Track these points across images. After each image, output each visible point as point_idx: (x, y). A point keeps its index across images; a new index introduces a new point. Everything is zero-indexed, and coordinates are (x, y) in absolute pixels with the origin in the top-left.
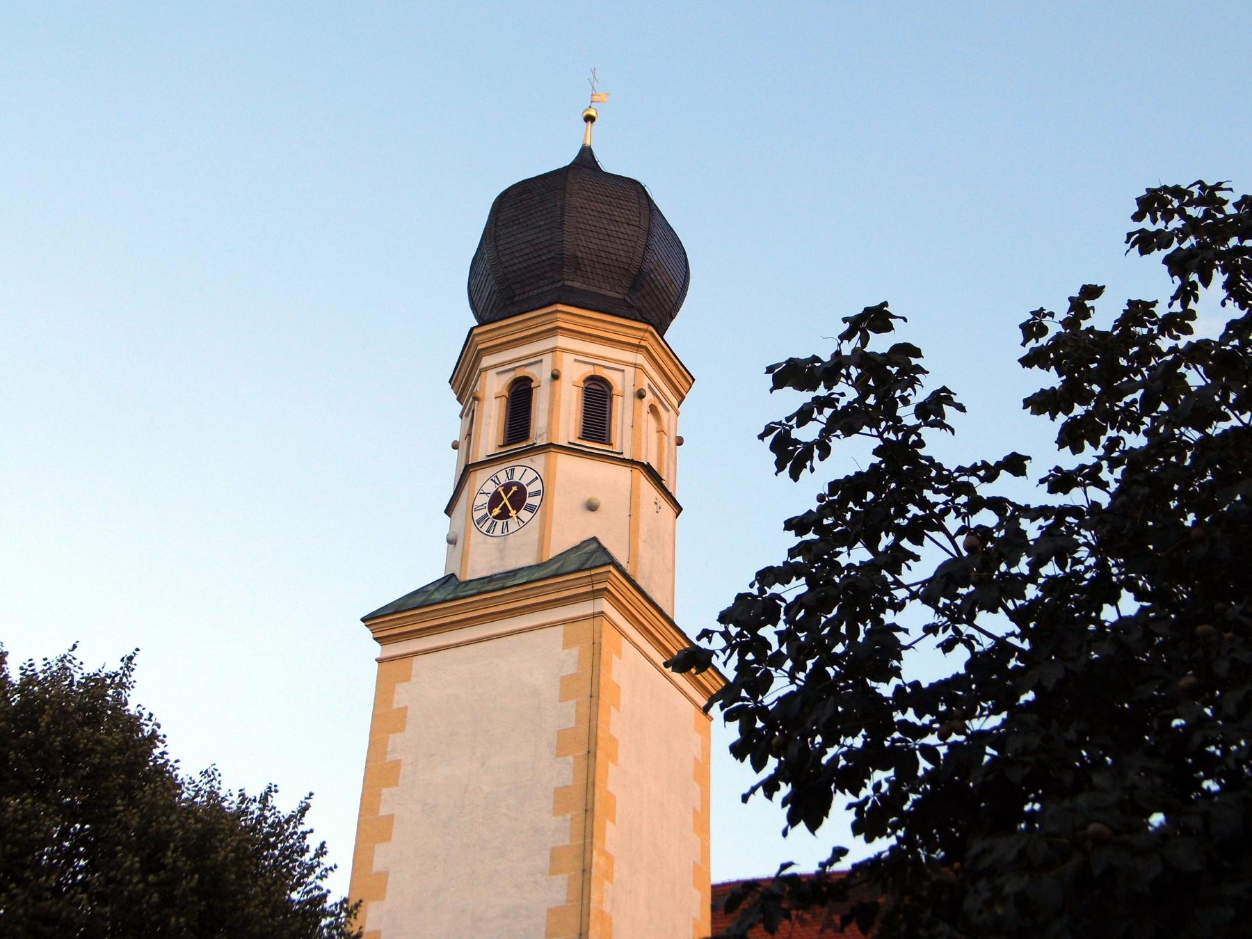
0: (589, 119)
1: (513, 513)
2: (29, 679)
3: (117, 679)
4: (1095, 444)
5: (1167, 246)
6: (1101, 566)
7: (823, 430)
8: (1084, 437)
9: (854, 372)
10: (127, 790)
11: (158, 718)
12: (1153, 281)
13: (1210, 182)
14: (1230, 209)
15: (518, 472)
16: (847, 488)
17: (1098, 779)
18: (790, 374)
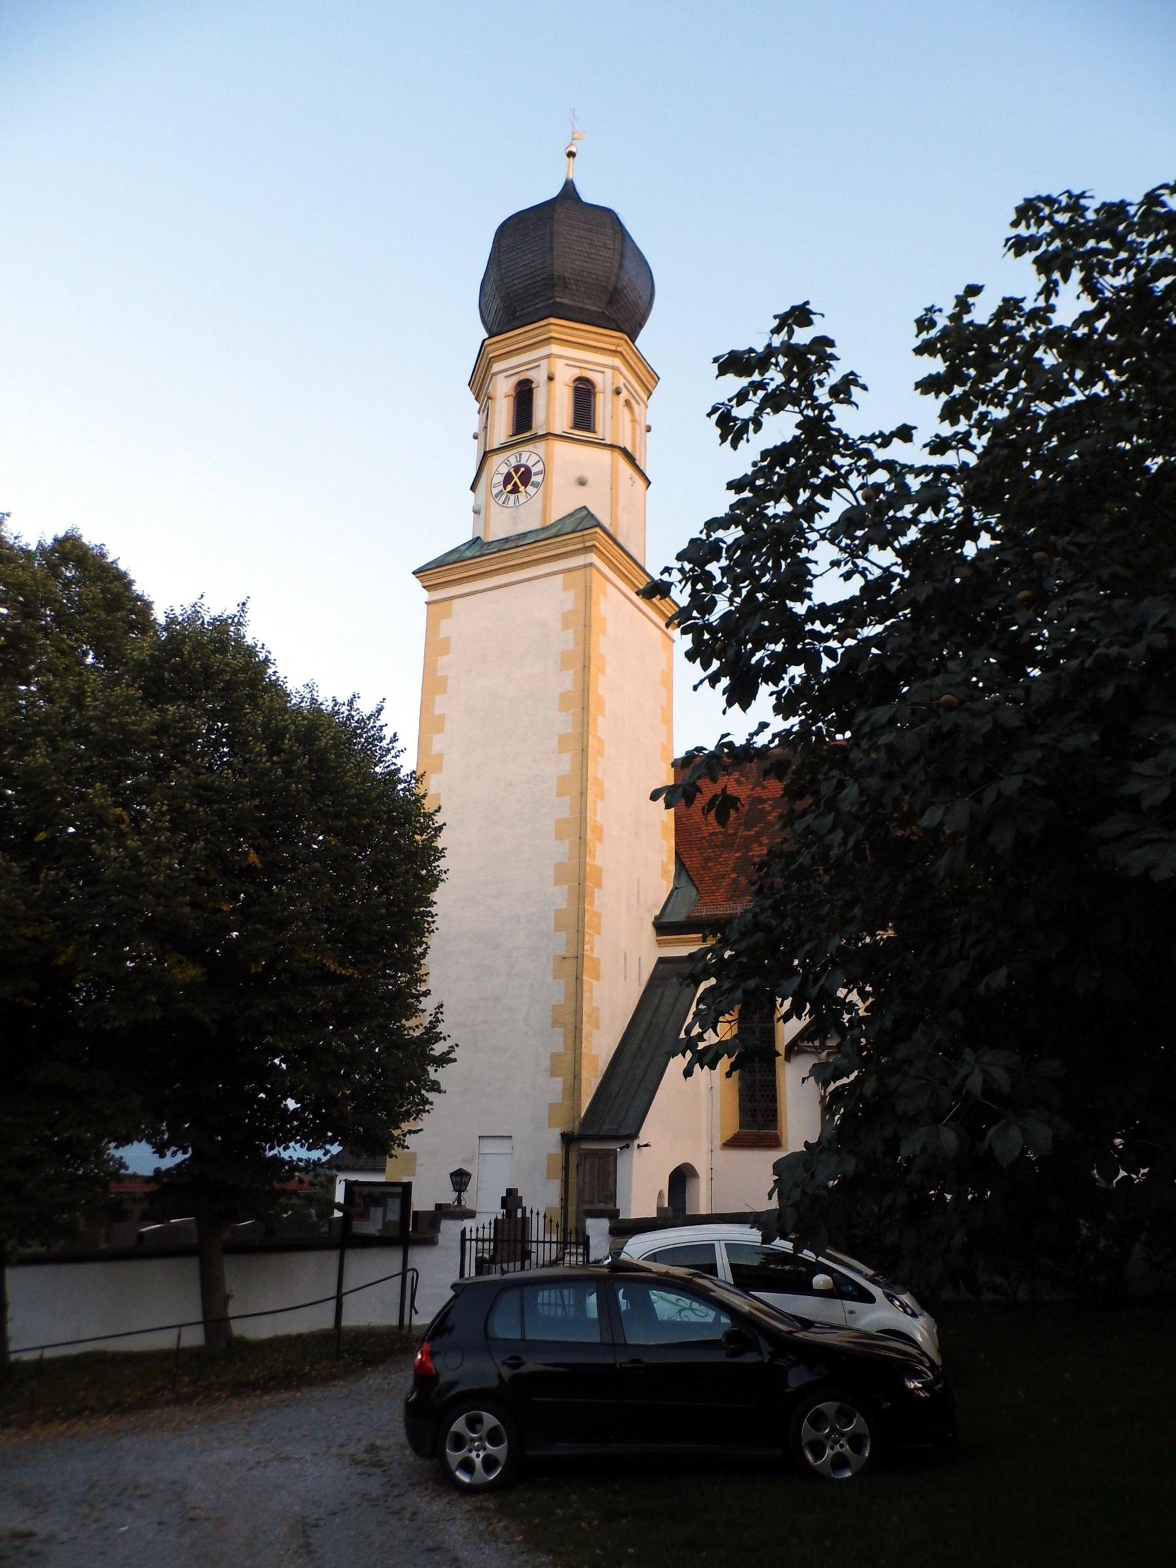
0: (571, 155)
1: (522, 488)
2: (172, 621)
3: (236, 620)
4: (969, 418)
5: (1037, 248)
6: (968, 514)
7: (757, 409)
8: (959, 412)
9: (782, 360)
10: (252, 698)
11: (268, 647)
12: (1021, 279)
13: (1076, 191)
14: (1090, 215)
15: (525, 456)
16: (776, 455)
17: (951, 665)
18: (733, 363)
